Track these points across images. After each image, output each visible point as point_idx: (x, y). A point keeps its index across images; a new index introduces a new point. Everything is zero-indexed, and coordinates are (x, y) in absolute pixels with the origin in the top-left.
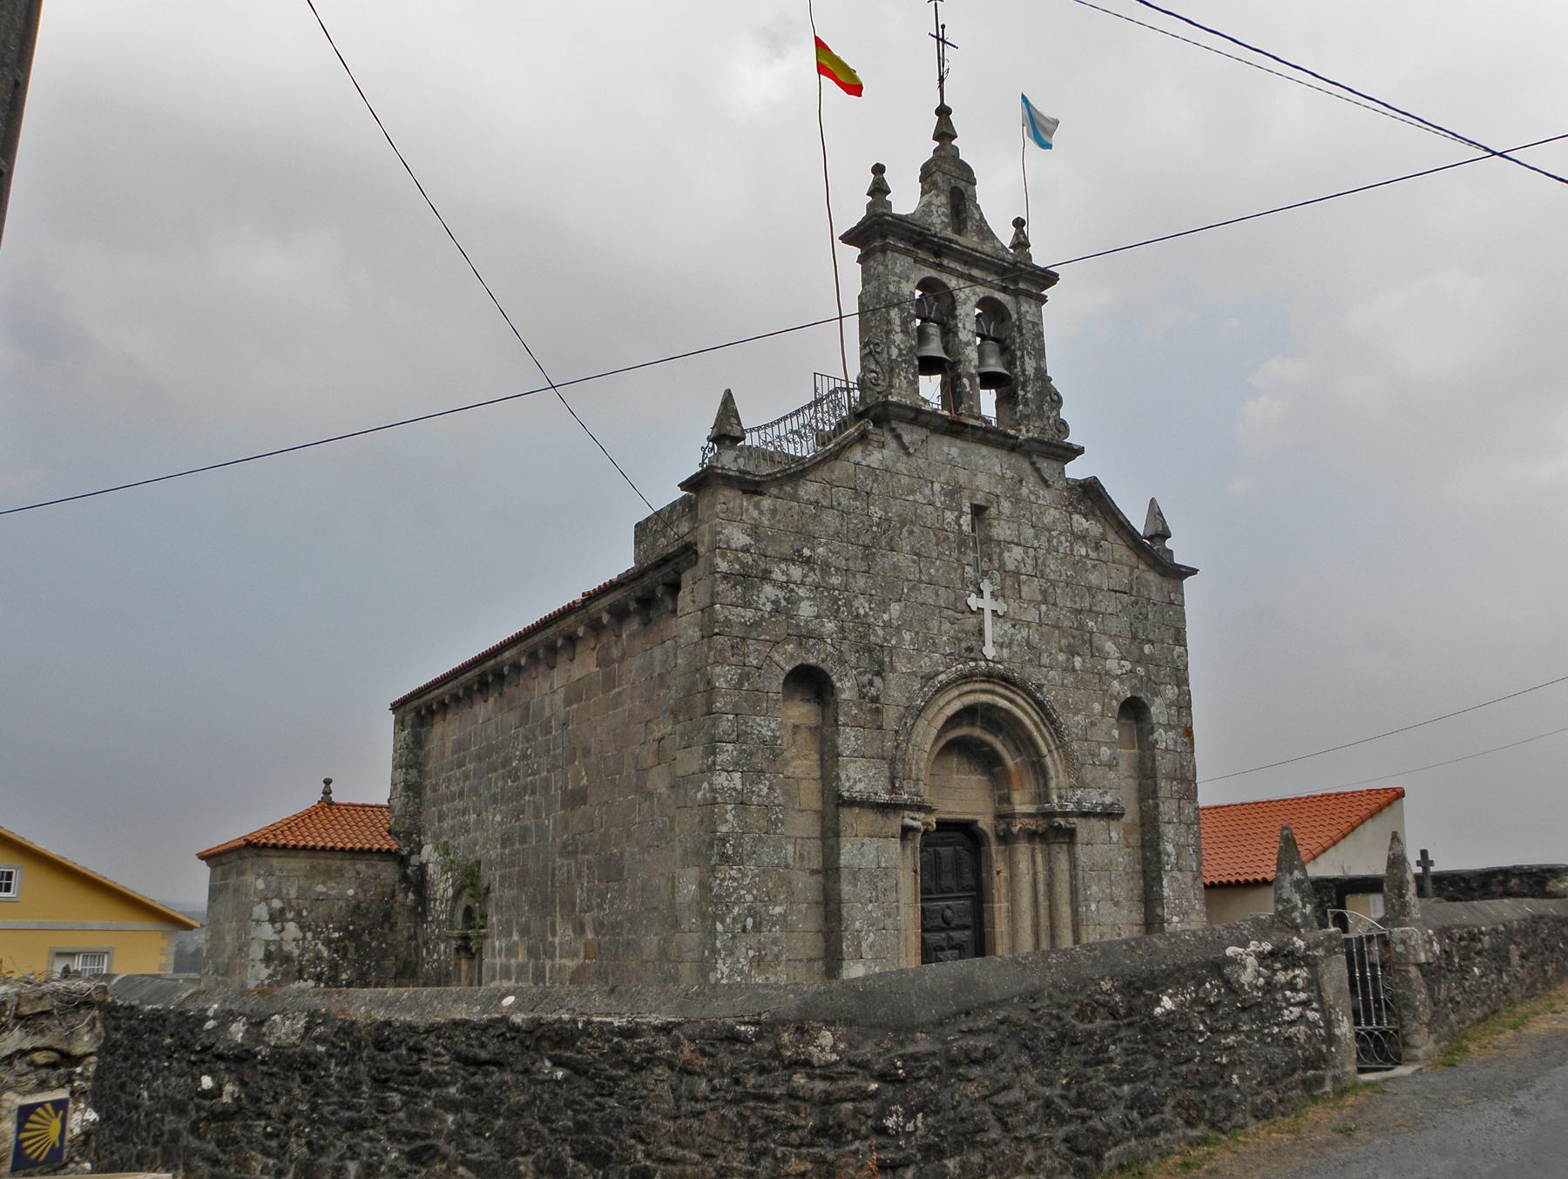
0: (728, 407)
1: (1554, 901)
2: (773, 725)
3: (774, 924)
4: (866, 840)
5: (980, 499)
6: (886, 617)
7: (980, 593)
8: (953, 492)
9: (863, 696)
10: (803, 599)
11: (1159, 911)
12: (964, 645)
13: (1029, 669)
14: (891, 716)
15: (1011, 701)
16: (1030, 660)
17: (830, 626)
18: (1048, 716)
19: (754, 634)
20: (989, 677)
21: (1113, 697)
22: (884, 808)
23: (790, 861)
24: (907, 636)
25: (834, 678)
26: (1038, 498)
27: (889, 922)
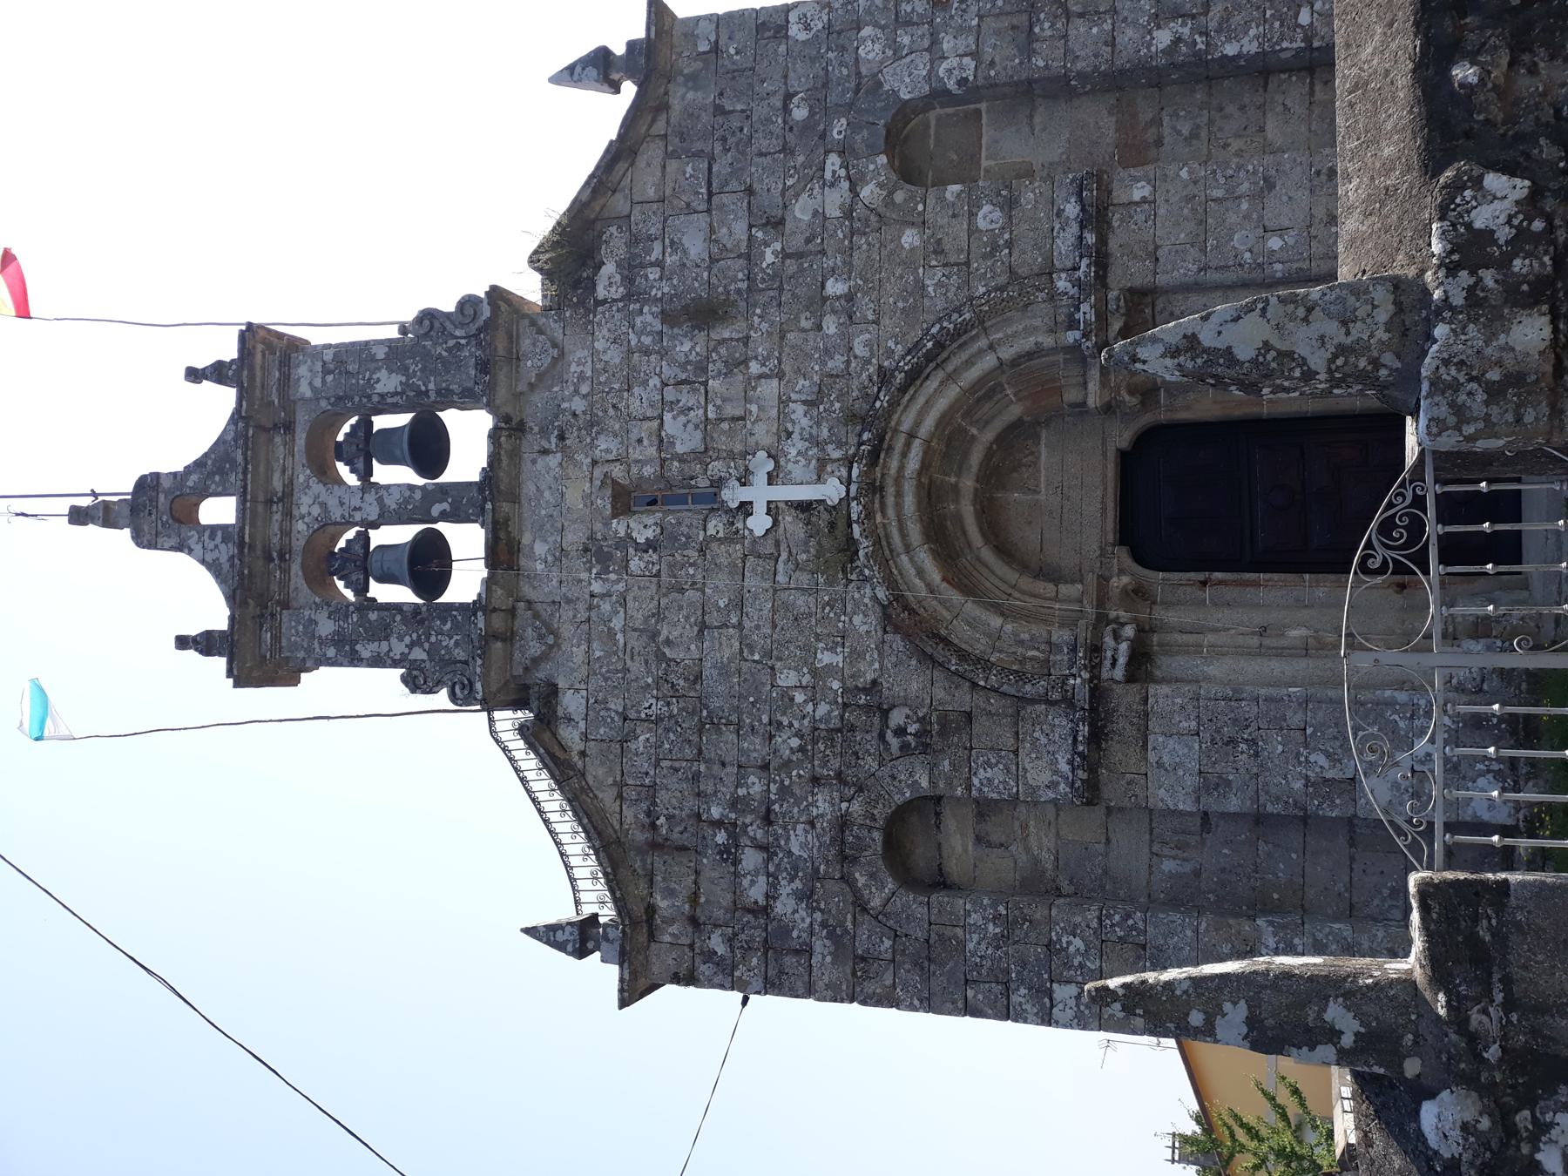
0: (548, 934)
4: (1152, 757)
5: (604, 503)
6: (799, 697)
7: (746, 508)
8: (599, 554)
9: (925, 748)
11: (1283, 55)
15: (912, 436)
18: (930, 356)
20: (873, 489)
21: (889, 201)
24: (825, 658)
26: (581, 377)
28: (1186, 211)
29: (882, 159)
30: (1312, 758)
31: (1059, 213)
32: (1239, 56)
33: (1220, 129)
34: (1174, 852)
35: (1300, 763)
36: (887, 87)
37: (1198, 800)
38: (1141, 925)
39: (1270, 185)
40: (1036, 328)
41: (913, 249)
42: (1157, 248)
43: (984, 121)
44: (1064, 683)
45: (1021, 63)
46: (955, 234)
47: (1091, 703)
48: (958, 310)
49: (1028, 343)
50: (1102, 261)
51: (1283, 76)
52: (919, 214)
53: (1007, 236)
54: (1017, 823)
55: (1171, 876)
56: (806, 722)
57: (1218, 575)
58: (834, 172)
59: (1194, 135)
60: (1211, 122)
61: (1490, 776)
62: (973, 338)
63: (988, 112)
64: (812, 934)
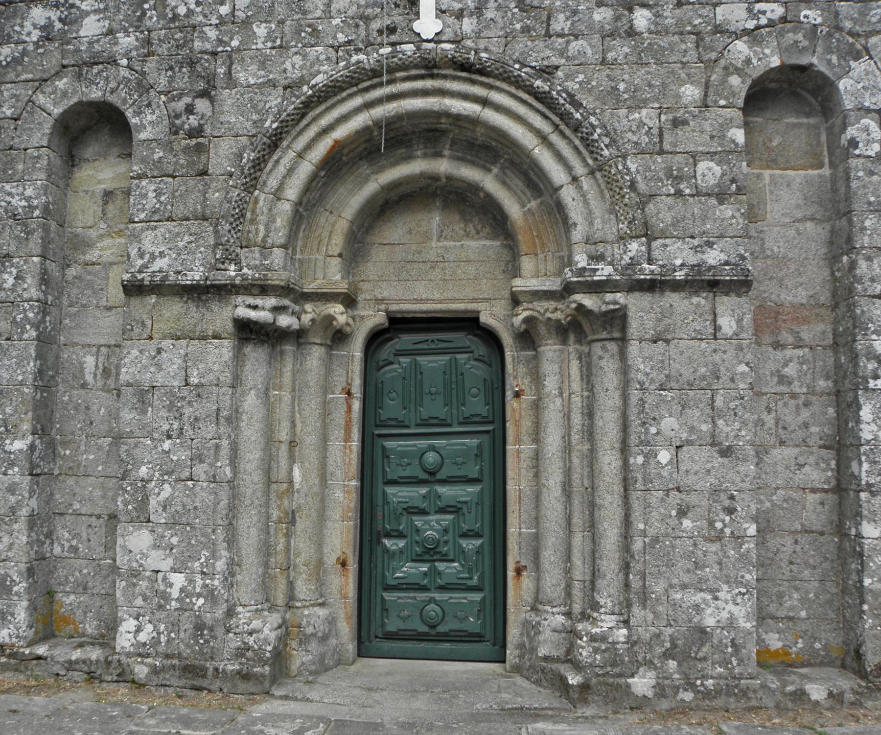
1: (443, 469)
2: (29, 192)
3: (12, 464)
4: (167, 344)
9: (175, 131)
10: (87, 14)
11: (854, 465)
12: (375, 25)
13: (520, 45)
14: (222, 156)
15: (485, 102)
16: (526, 30)
17: (127, 41)
18: (565, 117)
19: (11, 76)
20: (430, 67)
22: (201, 293)
23: (89, 378)
24: (261, 30)
25: (129, 114)
27: (200, 470)
28: (703, 370)
29: (775, 62)
30: (166, 486)
31: (710, 244)
32: (858, 421)
33: (785, 405)
34: (100, 365)
35: (162, 475)
36: (853, 64)
37: (129, 385)
38: (26, 336)
39: (726, 452)
40: (591, 224)
41: (678, 96)
42: (668, 342)
43: (810, 172)
44: (231, 260)
45: (870, 203)
46: (691, 138)
47: (213, 286)
48: (613, 141)
49: (575, 212)
50: (652, 286)
51: (833, 463)
52: (716, 102)
53: (687, 191)
54: (122, 226)
55: (81, 364)
56: (200, 18)
57: (357, 405)
58: (764, 13)
59: (783, 379)
60: (794, 396)
61: (155, 634)
62: (584, 160)
63: (821, 176)
64: (17, 43)
